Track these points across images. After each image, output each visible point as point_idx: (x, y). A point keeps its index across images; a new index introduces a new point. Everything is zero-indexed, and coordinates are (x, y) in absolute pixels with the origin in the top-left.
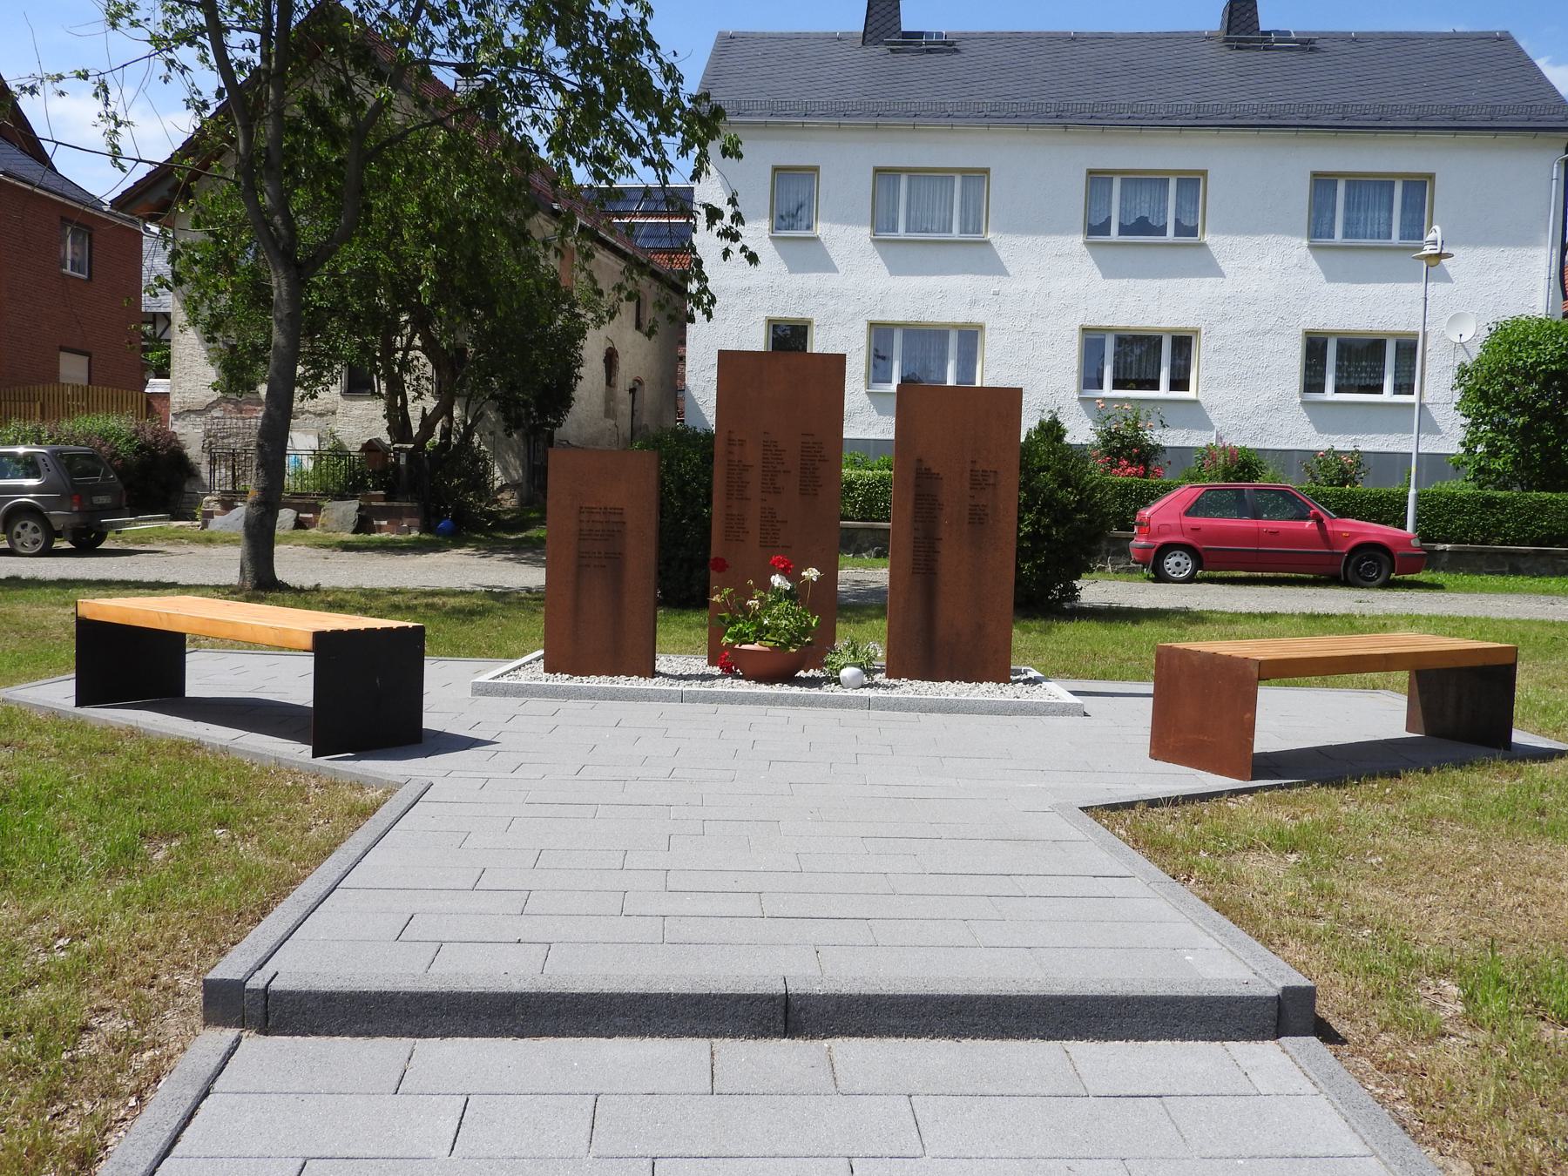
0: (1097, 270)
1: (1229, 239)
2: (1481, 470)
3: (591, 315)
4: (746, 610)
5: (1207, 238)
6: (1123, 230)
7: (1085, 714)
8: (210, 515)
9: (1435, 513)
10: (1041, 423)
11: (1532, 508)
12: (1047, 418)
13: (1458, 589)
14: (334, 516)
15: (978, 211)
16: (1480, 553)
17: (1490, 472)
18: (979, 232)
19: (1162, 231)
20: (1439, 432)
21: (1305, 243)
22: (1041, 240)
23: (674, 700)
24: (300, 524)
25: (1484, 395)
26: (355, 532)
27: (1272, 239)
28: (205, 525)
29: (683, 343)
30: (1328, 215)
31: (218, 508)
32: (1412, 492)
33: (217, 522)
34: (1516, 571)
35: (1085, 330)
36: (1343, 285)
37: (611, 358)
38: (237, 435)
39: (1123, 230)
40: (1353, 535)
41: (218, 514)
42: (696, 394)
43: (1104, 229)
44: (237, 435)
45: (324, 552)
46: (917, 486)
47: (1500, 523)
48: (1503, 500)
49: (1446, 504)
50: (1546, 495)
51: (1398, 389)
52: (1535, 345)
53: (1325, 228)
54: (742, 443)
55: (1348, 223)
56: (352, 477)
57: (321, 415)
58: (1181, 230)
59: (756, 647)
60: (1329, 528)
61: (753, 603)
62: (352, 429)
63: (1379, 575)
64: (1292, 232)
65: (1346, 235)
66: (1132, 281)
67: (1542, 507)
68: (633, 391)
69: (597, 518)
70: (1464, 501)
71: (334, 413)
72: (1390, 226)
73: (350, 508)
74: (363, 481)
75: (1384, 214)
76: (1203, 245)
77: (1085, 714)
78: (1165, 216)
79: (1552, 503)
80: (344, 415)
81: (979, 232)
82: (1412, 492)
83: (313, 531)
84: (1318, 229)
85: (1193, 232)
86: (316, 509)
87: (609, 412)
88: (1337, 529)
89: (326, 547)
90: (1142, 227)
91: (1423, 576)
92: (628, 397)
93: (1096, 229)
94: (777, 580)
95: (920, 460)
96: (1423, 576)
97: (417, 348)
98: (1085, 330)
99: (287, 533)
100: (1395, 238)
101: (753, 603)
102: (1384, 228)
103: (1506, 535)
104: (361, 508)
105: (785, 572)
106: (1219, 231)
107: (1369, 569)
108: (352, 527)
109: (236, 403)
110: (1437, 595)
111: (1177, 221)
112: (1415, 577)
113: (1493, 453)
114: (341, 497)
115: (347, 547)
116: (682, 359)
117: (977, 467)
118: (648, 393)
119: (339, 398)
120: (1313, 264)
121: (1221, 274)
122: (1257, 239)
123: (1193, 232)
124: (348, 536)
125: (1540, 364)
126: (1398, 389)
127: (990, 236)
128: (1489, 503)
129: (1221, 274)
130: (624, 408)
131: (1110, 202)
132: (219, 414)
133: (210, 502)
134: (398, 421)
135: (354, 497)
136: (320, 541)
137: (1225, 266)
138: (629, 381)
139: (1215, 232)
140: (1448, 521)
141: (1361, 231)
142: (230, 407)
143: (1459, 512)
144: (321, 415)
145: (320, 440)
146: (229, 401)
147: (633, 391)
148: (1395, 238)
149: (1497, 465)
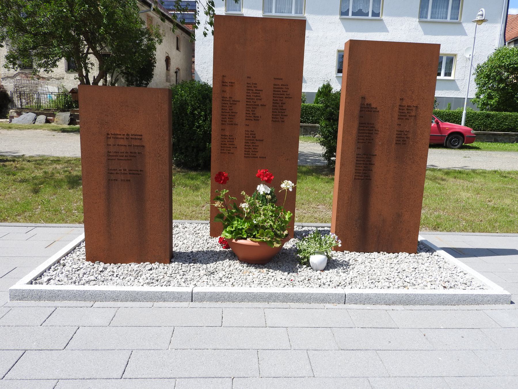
0: (344, 29)
1: (391, 18)
2: (484, 104)
3: (156, 39)
4: (240, 211)
5: (383, 18)
6: (354, 14)
7: (512, 303)
8: (12, 117)
9: (471, 119)
10: (324, 85)
11: (503, 118)
12: (325, 83)
13: (486, 149)
14: (61, 118)
15: (301, 5)
16: (484, 134)
17: (487, 104)
18: (302, 13)
19: (367, 15)
20: (459, 90)
21: (418, 20)
22: (324, 17)
23: (185, 300)
24: (48, 121)
25: (488, 76)
26: (69, 124)
27: (406, 18)
28: (11, 121)
29: (194, 57)
30: (426, 10)
31: (15, 114)
32: (464, 112)
33: (15, 120)
34: (496, 141)
35: (339, 51)
36: (430, 36)
37: (168, 60)
38: (27, 86)
39: (354, 14)
40: (450, 129)
41: (16, 117)
42: (199, 73)
43: (346, 13)
44: (27, 86)
45: (54, 133)
46: (361, 117)
47: (491, 123)
48: (493, 115)
49: (473, 116)
50: (508, 113)
51: (446, 75)
52: (509, 57)
53: (424, 15)
54: (232, 84)
55: (432, 13)
56: (67, 103)
57: (58, 79)
58: (374, 14)
59: (248, 242)
60: (441, 126)
61: (244, 206)
62: (70, 84)
63: (458, 144)
64: (413, 16)
65: (431, 18)
66: (356, 33)
67: (506, 118)
68: (176, 72)
69: (122, 142)
70: (479, 115)
71: (63, 78)
72: (447, 14)
73: (67, 115)
74: (72, 105)
75: (445, 10)
76: (382, 20)
77: (512, 303)
78: (368, 9)
79: (510, 116)
80: (67, 79)
81: (302, 13)
82: (464, 112)
83: (53, 124)
84: (422, 15)
85: (378, 15)
86: (54, 115)
87: (168, 80)
88: (444, 126)
89: (55, 130)
90: (359, 13)
91: (475, 144)
92: (174, 75)
93: (344, 13)
94: (262, 189)
95: (363, 98)
96: (475, 144)
97: (90, 53)
98: (339, 51)
99: (42, 124)
100: (449, 19)
101: (244, 206)
102: (444, 15)
103: (493, 127)
104: (71, 115)
105: (268, 183)
106: (387, 15)
107: (454, 142)
108: (68, 123)
109: (26, 74)
110: (479, 152)
111: (373, 11)
112: (470, 145)
113: (490, 97)
114: (63, 111)
115: (64, 131)
116: (194, 62)
117: (404, 103)
118: (182, 74)
119: (65, 72)
120: (420, 28)
121: (388, 31)
122: (401, 18)
123: (378, 15)
124: (66, 126)
125: (511, 65)
126: (446, 75)
127: (306, 15)
128: (488, 116)
129: (388, 31)
130: (173, 78)
131: (349, 3)
132: (19, 78)
133: (12, 112)
134: (84, 80)
135: (68, 111)
136: (53, 128)
137: (389, 28)
138: (175, 69)
139: (386, 15)
140: (473, 123)
141: (437, 16)
142: (23, 76)
143: (477, 119)
144: (58, 79)
145: (59, 89)
146: (22, 73)
147: (176, 72)
148: (449, 19)
149: (492, 102)
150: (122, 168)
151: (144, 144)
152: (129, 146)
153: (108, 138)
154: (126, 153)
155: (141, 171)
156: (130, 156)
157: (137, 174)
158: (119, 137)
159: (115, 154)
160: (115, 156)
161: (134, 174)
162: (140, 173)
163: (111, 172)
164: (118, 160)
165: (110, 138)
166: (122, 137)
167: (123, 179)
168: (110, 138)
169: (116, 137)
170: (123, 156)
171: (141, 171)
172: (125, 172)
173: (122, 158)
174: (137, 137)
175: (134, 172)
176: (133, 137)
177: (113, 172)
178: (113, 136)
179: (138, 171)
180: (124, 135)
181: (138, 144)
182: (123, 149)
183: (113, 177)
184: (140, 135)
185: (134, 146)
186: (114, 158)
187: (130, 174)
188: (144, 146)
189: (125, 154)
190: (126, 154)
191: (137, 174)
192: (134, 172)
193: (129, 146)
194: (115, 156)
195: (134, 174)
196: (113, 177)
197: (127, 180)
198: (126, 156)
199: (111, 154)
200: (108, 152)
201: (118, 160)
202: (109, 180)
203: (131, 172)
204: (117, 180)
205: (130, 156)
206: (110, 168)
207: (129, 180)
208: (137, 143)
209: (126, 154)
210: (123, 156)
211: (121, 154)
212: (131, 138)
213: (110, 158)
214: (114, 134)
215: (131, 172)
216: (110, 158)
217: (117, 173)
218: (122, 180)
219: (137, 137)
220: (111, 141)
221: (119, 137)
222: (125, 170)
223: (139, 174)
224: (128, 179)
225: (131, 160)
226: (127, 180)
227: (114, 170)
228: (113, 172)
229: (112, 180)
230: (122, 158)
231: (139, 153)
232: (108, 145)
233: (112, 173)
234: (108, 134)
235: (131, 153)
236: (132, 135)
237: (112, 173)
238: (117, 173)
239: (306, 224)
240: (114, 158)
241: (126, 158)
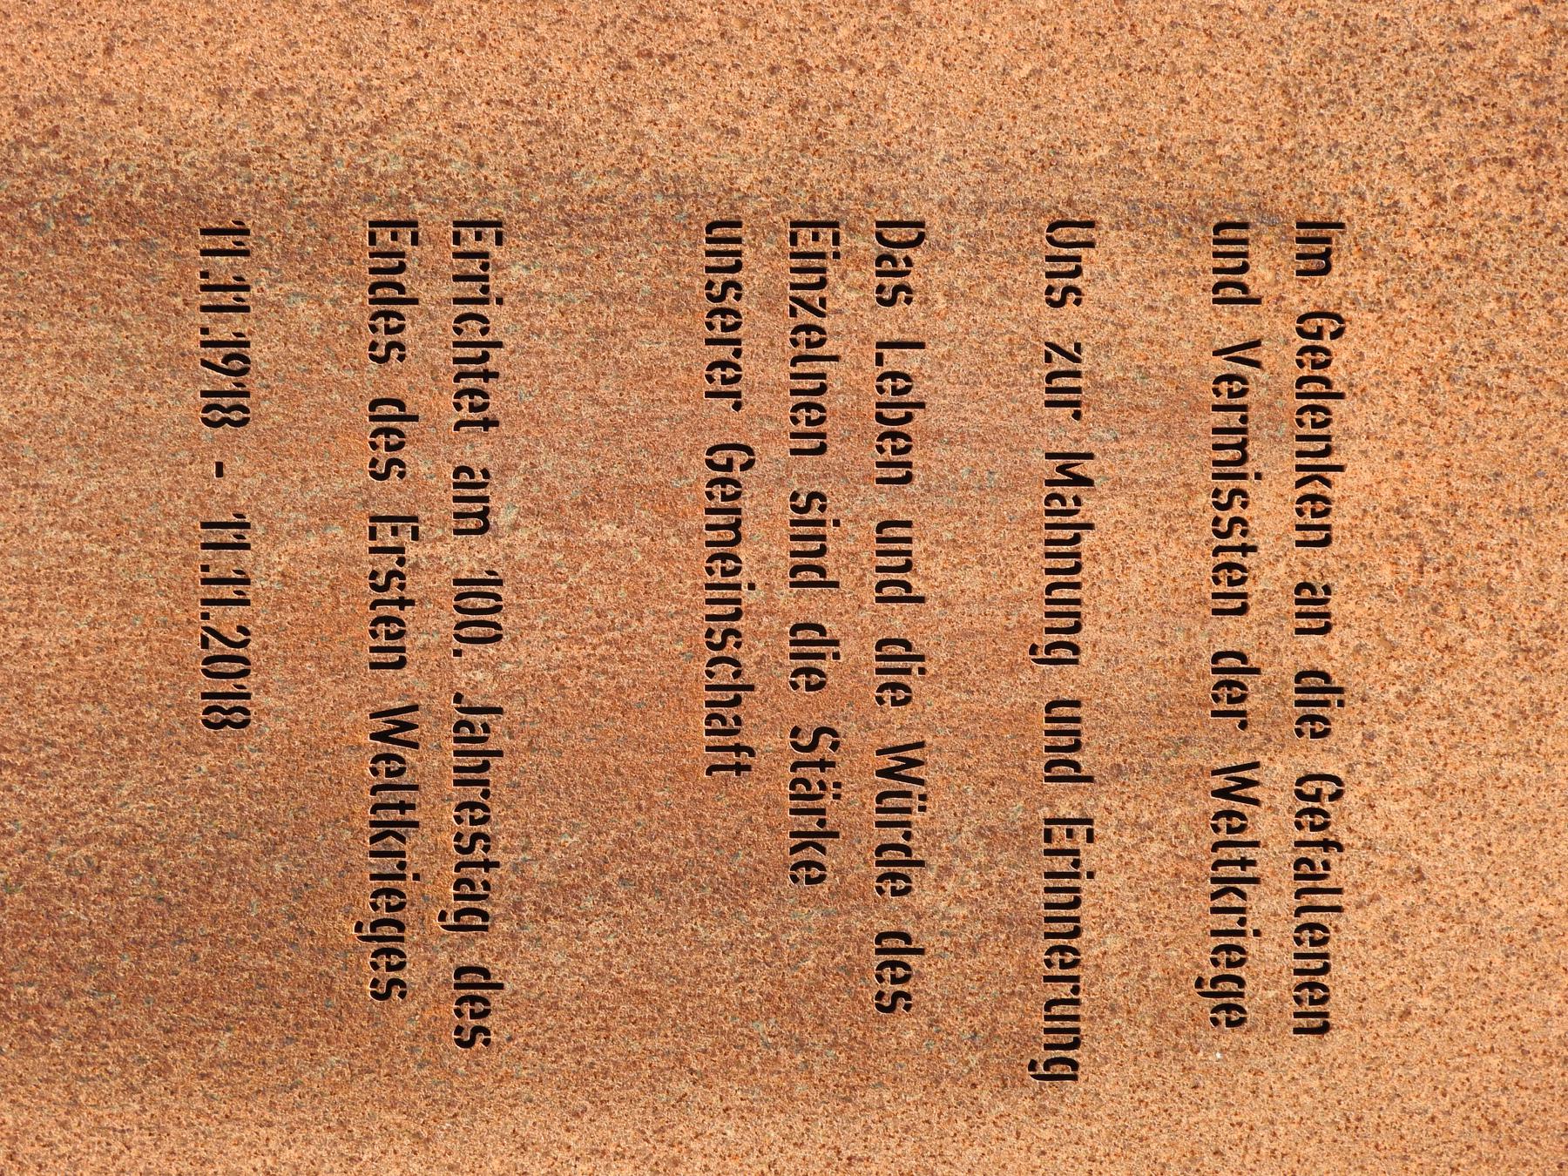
69: (1145, 557)
150: (515, 541)
151: (1105, 1071)
152: (1063, 718)
153: (1230, 237)
154: (898, 661)
155: (474, 986)
156: (814, 748)
157: (389, 890)
158: (1271, 507)
159: (851, 386)
160: (810, 401)
161: (391, 828)
162: (431, 959)
163: (432, 287)
164: (727, 467)
165: (1232, 290)
166: (1273, 572)
167: (266, 561)
168: (1232, 290)
169: (1275, 419)
170: (809, 571)
171: (474, 986)
172: (430, 626)
173: (766, 547)
174: (1272, 904)
175: (437, 821)
176: (1273, 826)
177: (430, 332)
178: (1280, 361)
179: (470, 918)
180: (1313, 606)
181: (1097, 944)
182: (978, 580)
183: (303, 320)
184: (1312, 985)
185: (1063, 841)
186: (767, 366)
187: (396, 727)
188: (1059, 1067)
189: (855, 617)
190: (856, 655)
191: (389, 890)
192: (437, 821)
193: (1063, 718)
194: (810, 401)
195: (391, 828)
196: (303, 320)
197: (227, 660)
198: (811, 642)
199: (850, 291)
200: (900, 240)
201: (727, 467)
202: (231, 236)
203: (433, 759)
204: (227, 410)
205: (814, 748)
206: (512, 269)
207: (227, 715)
208: (1141, 911)
209: (856, 655)
210: (809, 571)
211: (851, 550)
212: (1237, 785)
213: (765, 268)
214: (1317, 393)
215: (433, 759)
216: (765, 268)
217: (391, 420)
218: (230, 533)
219: (1272, 904)
220: (1153, 317)
221: (1271, 507)
222: (479, 609)
223: (386, 938)
224: (268, 697)
225: (734, 758)
226: (227, 660)
227: (475, 369)
228: (430, 332)
229: (229, 297)
230: (766, 547)
231: (896, 950)
232: (1067, 242)
233: (389, 299)
234: (1317, 245)
235: (902, 764)
236: (1315, 799)
237: (389, 299)
238: (391, 420)
239: (978, 580)
240: (767, 366)
241: (764, 650)
